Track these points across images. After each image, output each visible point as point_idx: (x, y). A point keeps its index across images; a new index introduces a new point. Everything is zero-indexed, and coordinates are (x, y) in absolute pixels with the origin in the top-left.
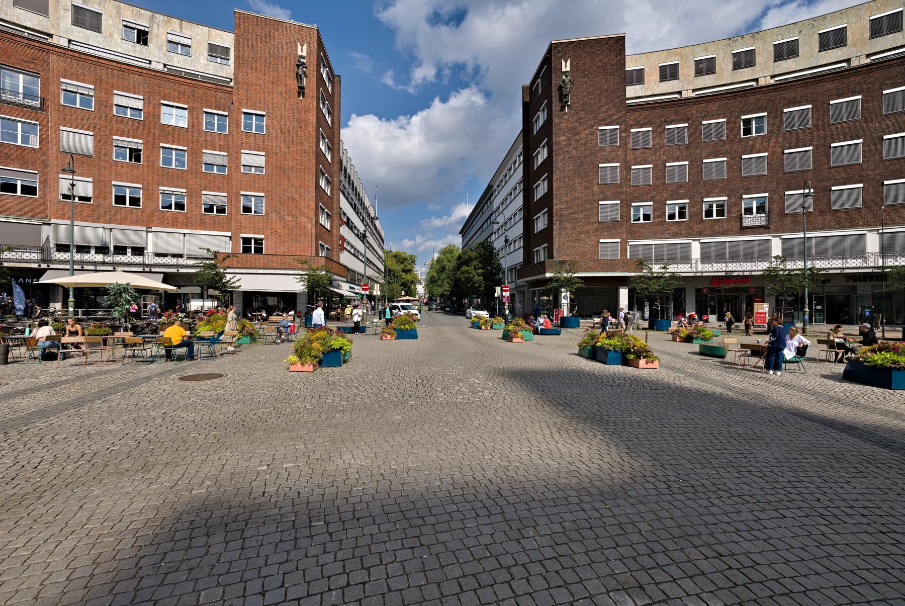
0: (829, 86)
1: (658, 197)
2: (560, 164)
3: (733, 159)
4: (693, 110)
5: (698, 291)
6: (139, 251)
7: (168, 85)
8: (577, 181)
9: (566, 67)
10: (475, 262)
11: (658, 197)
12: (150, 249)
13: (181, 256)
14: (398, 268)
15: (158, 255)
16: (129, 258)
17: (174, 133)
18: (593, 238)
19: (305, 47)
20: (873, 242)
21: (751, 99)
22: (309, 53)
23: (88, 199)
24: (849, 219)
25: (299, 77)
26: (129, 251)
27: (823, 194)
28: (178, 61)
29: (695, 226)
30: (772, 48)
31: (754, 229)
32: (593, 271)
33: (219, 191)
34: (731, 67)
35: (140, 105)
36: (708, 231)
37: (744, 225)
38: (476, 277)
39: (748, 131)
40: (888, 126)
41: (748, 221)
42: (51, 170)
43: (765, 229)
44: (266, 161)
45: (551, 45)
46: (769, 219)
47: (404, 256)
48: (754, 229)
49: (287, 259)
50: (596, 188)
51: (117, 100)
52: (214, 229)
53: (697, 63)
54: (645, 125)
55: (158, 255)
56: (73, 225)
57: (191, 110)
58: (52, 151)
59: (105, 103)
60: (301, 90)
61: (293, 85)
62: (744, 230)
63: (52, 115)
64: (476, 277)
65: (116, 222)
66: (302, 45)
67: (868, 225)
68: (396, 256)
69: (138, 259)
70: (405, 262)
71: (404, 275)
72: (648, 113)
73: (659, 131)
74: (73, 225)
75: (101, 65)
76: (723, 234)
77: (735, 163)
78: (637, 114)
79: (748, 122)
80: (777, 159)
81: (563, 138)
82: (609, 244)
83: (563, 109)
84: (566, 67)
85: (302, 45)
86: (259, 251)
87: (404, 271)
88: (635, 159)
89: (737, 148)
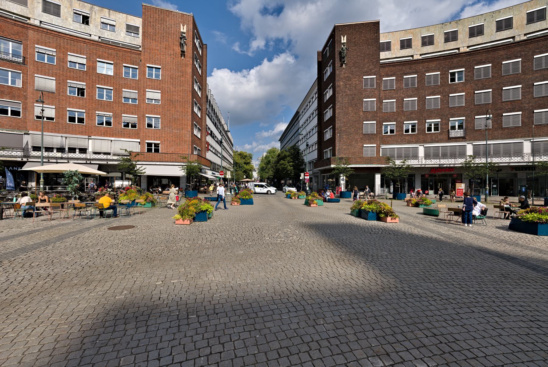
0: (502, 53)
1: (399, 119)
2: (340, 99)
3: (444, 96)
4: (420, 67)
5: (423, 176)
6: (83, 151)
7: (101, 49)
8: (350, 109)
9: (344, 40)
10: (288, 158)
11: (399, 119)
12: (90, 150)
13: (109, 154)
14: (241, 161)
15: (95, 153)
16: (77, 155)
17: (105, 79)
18: (360, 144)
19: (185, 27)
20: (527, 147)
21: (455, 60)
22: (188, 31)
23: (52, 119)
24: (513, 132)
25: (181, 45)
26: (77, 150)
27: (498, 118)
28: (108, 35)
29: (421, 137)
30: (468, 30)
31: (456, 139)
32: (359, 164)
33: (133, 114)
34: (443, 41)
35: (84, 61)
36: (429, 140)
37: (450, 136)
38: (289, 168)
39: (453, 80)
40: (537, 77)
41: (453, 134)
42: (29, 101)
43: (463, 139)
44: (162, 96)
45: (335, 28)
46: (465, 132)
47: (245, 154)
48: (456, 139)
49: (174, 156)
50: (361, 114)
51: (70, 58)
52: (129, 137)
53: (423, 38)
54: (391, 76)
55: (95, 153)
56: (43, 135)
57: (115, 65)
58: (30, 90)
59: (62, 60)
60: (183, 53)
61: (178, 50)
62: (450, 139)
63: (30, 67)
64: (289, 168)
65: (69, 133)
66: (183, 26)
67: (525, 137)
68: (240, 154)
69: (83, 156)
70: (246, 158)
71: (245, 166)
72: (393, 68)
73: (400, 79)
74: (43, 135)
75: (60, 37)
76: (437, 142)
77: (445, 99)
78: (387, 69)
79: (453, 74)
80: (470, 97)
81: (342, 83)
82: (369, 148)
83: (342, 65)
84: (344, 40)
85: (183, 26)
86: (157, 151)
87: (245, 163)
88: (385, 96)
89: (447, 89)
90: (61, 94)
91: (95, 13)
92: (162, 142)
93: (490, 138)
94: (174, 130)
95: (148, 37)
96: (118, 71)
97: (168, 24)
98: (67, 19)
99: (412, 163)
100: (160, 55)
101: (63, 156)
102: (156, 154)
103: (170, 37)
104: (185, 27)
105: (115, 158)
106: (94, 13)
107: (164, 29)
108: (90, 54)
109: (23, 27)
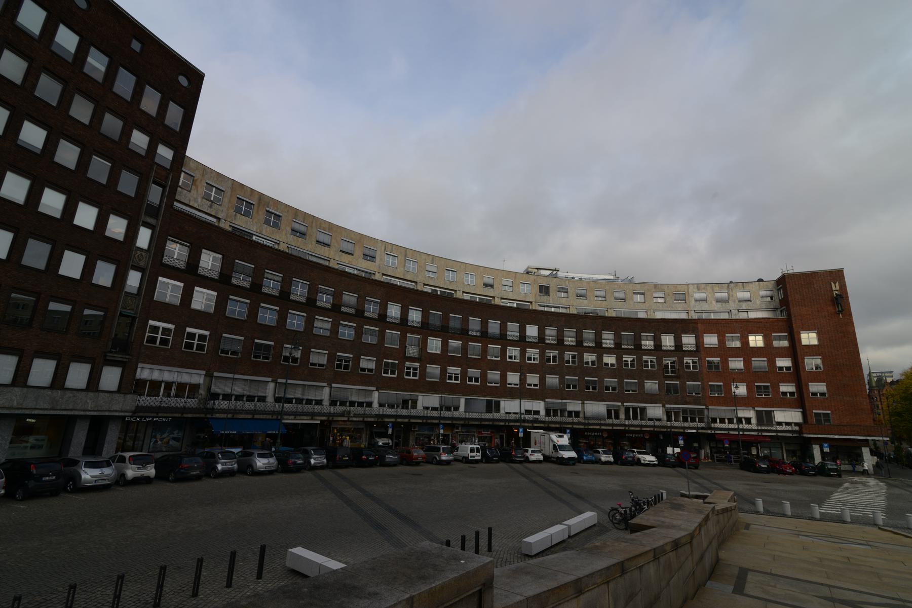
19: (837, 284)
26: (784, 424)
66: (835, 283)
85: (835, 283)
90: (725, 371)
91: (732, 290)
92: (832, 411)
93: (405, 462)
94: (845, 398)
95: (796, 304)
96: (769, 342)
97: (815, 286)
98: (711, 303)
99: (456, 414)
100: (813, 319)
101: (699, 426)
102: (723, 417)
103: (820, 298)
104: (837, 284)
105: (789, 428)
106: (730, 290)
107: (812, 293)
108: (742, 331)
109: (695, 323)
